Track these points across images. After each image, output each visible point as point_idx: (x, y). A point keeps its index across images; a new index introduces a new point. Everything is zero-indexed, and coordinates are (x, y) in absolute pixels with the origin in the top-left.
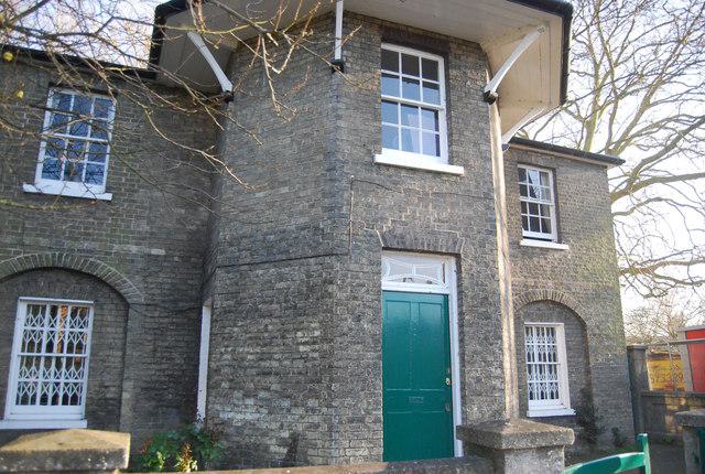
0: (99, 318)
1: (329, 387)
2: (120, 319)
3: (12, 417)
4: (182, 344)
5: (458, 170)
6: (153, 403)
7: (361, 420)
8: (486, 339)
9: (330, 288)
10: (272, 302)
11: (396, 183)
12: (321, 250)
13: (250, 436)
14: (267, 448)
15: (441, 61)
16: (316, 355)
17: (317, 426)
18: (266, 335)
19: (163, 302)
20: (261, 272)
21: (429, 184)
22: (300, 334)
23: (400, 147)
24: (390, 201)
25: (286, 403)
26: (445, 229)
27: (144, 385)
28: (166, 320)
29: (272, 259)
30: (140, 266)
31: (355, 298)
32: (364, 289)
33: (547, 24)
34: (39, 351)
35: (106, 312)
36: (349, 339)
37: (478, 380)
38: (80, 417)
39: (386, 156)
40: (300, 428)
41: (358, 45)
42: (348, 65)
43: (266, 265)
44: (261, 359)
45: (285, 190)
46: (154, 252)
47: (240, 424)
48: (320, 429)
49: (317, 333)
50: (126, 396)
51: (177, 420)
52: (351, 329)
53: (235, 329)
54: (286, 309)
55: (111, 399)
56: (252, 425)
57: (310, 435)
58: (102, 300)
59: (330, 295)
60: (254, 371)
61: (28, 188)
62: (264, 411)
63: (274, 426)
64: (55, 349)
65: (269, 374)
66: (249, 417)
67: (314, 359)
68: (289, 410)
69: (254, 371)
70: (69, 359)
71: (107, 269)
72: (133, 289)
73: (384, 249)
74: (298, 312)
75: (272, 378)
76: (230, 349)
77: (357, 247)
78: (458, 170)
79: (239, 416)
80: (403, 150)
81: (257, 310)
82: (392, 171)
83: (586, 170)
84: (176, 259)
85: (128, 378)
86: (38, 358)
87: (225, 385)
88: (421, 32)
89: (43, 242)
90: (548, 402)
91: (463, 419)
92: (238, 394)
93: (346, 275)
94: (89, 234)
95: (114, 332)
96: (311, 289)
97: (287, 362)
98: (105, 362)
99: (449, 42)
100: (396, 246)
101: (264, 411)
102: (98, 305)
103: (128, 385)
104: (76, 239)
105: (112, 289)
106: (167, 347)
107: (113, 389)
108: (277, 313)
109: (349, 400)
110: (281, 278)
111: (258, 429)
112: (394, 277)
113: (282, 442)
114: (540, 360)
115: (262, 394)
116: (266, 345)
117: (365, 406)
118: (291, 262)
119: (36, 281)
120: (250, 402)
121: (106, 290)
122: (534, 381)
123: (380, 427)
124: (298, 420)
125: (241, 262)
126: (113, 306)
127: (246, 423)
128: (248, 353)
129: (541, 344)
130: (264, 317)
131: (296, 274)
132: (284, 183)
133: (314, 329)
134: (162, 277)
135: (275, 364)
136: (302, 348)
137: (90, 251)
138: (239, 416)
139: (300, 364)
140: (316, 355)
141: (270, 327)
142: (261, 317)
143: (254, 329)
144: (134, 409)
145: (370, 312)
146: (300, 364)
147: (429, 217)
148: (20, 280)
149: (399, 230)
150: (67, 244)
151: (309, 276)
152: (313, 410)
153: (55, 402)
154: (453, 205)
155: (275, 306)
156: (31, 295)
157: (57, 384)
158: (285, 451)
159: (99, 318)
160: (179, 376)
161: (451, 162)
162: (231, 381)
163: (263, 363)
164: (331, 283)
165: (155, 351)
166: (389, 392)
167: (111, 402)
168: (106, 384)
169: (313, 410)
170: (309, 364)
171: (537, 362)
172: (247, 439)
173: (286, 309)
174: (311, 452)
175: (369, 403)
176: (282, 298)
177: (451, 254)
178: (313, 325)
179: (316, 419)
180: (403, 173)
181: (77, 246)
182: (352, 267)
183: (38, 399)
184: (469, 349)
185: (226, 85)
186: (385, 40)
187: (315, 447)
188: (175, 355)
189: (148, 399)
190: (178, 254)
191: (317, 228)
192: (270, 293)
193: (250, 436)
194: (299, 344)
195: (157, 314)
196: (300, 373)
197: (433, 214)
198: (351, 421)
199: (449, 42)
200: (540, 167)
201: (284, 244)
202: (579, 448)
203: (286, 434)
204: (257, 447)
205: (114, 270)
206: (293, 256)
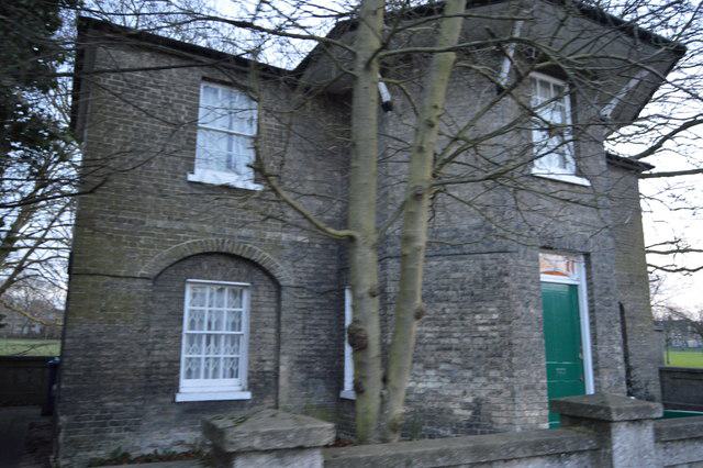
0: (255, 298)
1: (509, 361)
2: (272, 300)
4: (326, 322)
5: (586, 182)
6: (304, 375)
7: (533, 387)
9: (506, 280)
10: (448, 289)
12: (495, 248)
13: (433, 402)
14: (450, 412)
16: (494, 334)
17: (500, 392)
18: (444, 317)
19: (309, 284)
20: (435, 263)
22: (478, 316)
25: (468, 374)
27: (296, 358)
29: (445, 252)
30: (289, 252)
31: (524, 288)
32: (530, 281)
35: (261, 293)
38: (240, 388)
40: (483, 394)
43: (441, 258)
44: (441, 337)
46: (300, 239)
47: (422, 392)
48: (503, 395)
49: (495, 316)
50: (283, 369)
51: (324, 390)
54: (463, 295)
55: (268, 372)
56: (435, 392)
57: (493, 400)
58: (257, 283)
59: (506, 285)
60: (433, 347)
61: (191, 178)
62: (446, 380)
63: (457, 393)
65: (450, 349)
66: (430, 385)
68: (471, 380)
69: (433, 347)
70: (209, 336)
71: (262, 255)
72: (285, 273)
74: (475, 298)
75: (453, 353)
78: (259, 188)
81: (433, 296)
82: (542, 182)
84: (317, 246)
85: (284, 354)
86: (200, 336)
89: (208, 228)
90: (240, 363)
91: (596, 387)
94: (246, 223)
95: (268, 312)
96: (487, 279)
97: (467, 340)
98: (261, 338)
102: (255, 287)
103: (284, 359)
105: (266, 272)
106: (314, 325)
107: (268, 363)
109: (525, 372)
111: (441, 396)
113: (466, 406)
115: (443, 366)
116: (443, 325)
119: (200, 264)
120: (431, 373)
121: (259, 273)
123: (545, 393)
124: (480, 388)
126: (265, 288)
127: (428, 391)
128: (426, 332)
130: (441, 302)
131: (470, 268)
133: (493, 313)
134: (307, 262)
136: (481, 328)
137: (248, 238)
139: (480, 341)
140: (494, 334)
141: (448, 311)
142: (436, 301)
144: (290, 379)
146: (480, 341)
148: (190, 262)
150: (228, 231)
152: (495, 379)
155: (450, 293)
156: (204, 278)
157: (216, 359)
158: (470, 413)
159: (255, 298)
160: (325, 351)
163: (442, 341)
164: (507, 275)
165: (304, 328)
167: (268, 374)
168: (264, 358)
169: (495, 379)
170: (489, 342)
172: (430, 404)
173: (463, 295)
174: (495, 414)
176: (458, 286)
178: (491, 309)
179: (499, 386)
181: (237, 232)
182: (522, 262)
183: (211, 374)
184: (601, 329)
187: (499, 409)
188: (320, 332)
189: (301, 371)
190: (319, 241)
193: (433, 402)
194: (477, 325)
195: (305, 295)
196: (480, 349)
198: (526, 388)
203: (469, 399)
204: (441, 411)
205: (268, 255)
206: (467, 251)
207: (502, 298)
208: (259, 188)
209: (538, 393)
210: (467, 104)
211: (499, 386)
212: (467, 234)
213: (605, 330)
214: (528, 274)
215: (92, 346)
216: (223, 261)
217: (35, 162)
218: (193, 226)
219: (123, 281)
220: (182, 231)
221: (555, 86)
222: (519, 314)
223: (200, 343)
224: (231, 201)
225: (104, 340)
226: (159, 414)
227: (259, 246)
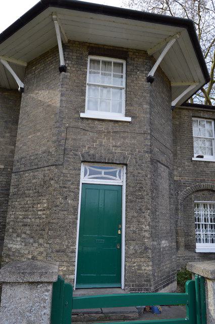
1: (48, 233)
3: (199, 248)
15: (124, 63)
16: (44, 216)
20: (27, 175)
21: (118, 128)
22: (39, 206)
23: (99, 109)
25: (31, 241)
26: (119, 150)
28: (3, 199)
31: (65, 187)
33: (179, 33)
34: (208, 222)
36: (60, 209)
39: (88, 114)
40: (36, 254)
41: (75, 57)
42: (69, 68)
43: (30, 171)
45: (39, 134)
49: (45, 205)
52: (61, 203)
53: (16, 203)
61: (82, 115)
63: (26, 252)
64: (209, 221)
66: (18, 247)
67: (44, 218)
73: (82, 162)
74: (40, 194)
75: (27, 228)
76: (14, 213)
77: (68, 161)
78: (129, 119)
79: (15, 246)
80: (112, 112)
82: (90, 121)
87: (11, 230)
88: (111, 48)
92: (15, 235)
93: (60, 176)
99: (128, 52)
100: (89, 160)
101: (23, 244)
106: (3, 212)
108: (31, 195)
109: (58, 240)
110: (34, 178)
112: (91, 176)
114: (205, 221)
115: (23, 236)
116: (26, 211)
117: (67, 244)
118: (38, 169)
120: (19, 239)
122: (201, 233)
125: (21, 170)
129: (206, 213)
131: (40, 174)
132: (39, 131)
135: (29, 220)
136: (39, 213)
138: (15, 246)
140: (44, 216)
141: (29, 202)
143: (23, 203)
145: (72, 194)
147: (109, 145)
149: (92, 152)
151: (44, 176)
153: (206, 242)
154: (124, 138)
161: (126, 116)
162: (13, 228)
163: (24, 220)
169: (41, 245)
170: (41, 221)
171: (210, 223)
175: (69, 242)
178: (44, 201)
179: (42, 249)
180: (96, 122)
182: (64, 171)
185: (20, 84)
186: (91, 53)
191: (49, 152)
192: (29, 185)
197: (112, 142)
198: (58, 251)
199: (128, 52)
200: (207, 118)
201: (36, 161)
206: (39, 166)
207: (49, 194)
208: (129, 119)
209: (66, 255)
210: (49, 81)
211: (42, 249)
212: (41, 156)
213: (136, 214)
214: (69, 179)
221: (114, 63)
222: (58, 203)
223: (199, 228)
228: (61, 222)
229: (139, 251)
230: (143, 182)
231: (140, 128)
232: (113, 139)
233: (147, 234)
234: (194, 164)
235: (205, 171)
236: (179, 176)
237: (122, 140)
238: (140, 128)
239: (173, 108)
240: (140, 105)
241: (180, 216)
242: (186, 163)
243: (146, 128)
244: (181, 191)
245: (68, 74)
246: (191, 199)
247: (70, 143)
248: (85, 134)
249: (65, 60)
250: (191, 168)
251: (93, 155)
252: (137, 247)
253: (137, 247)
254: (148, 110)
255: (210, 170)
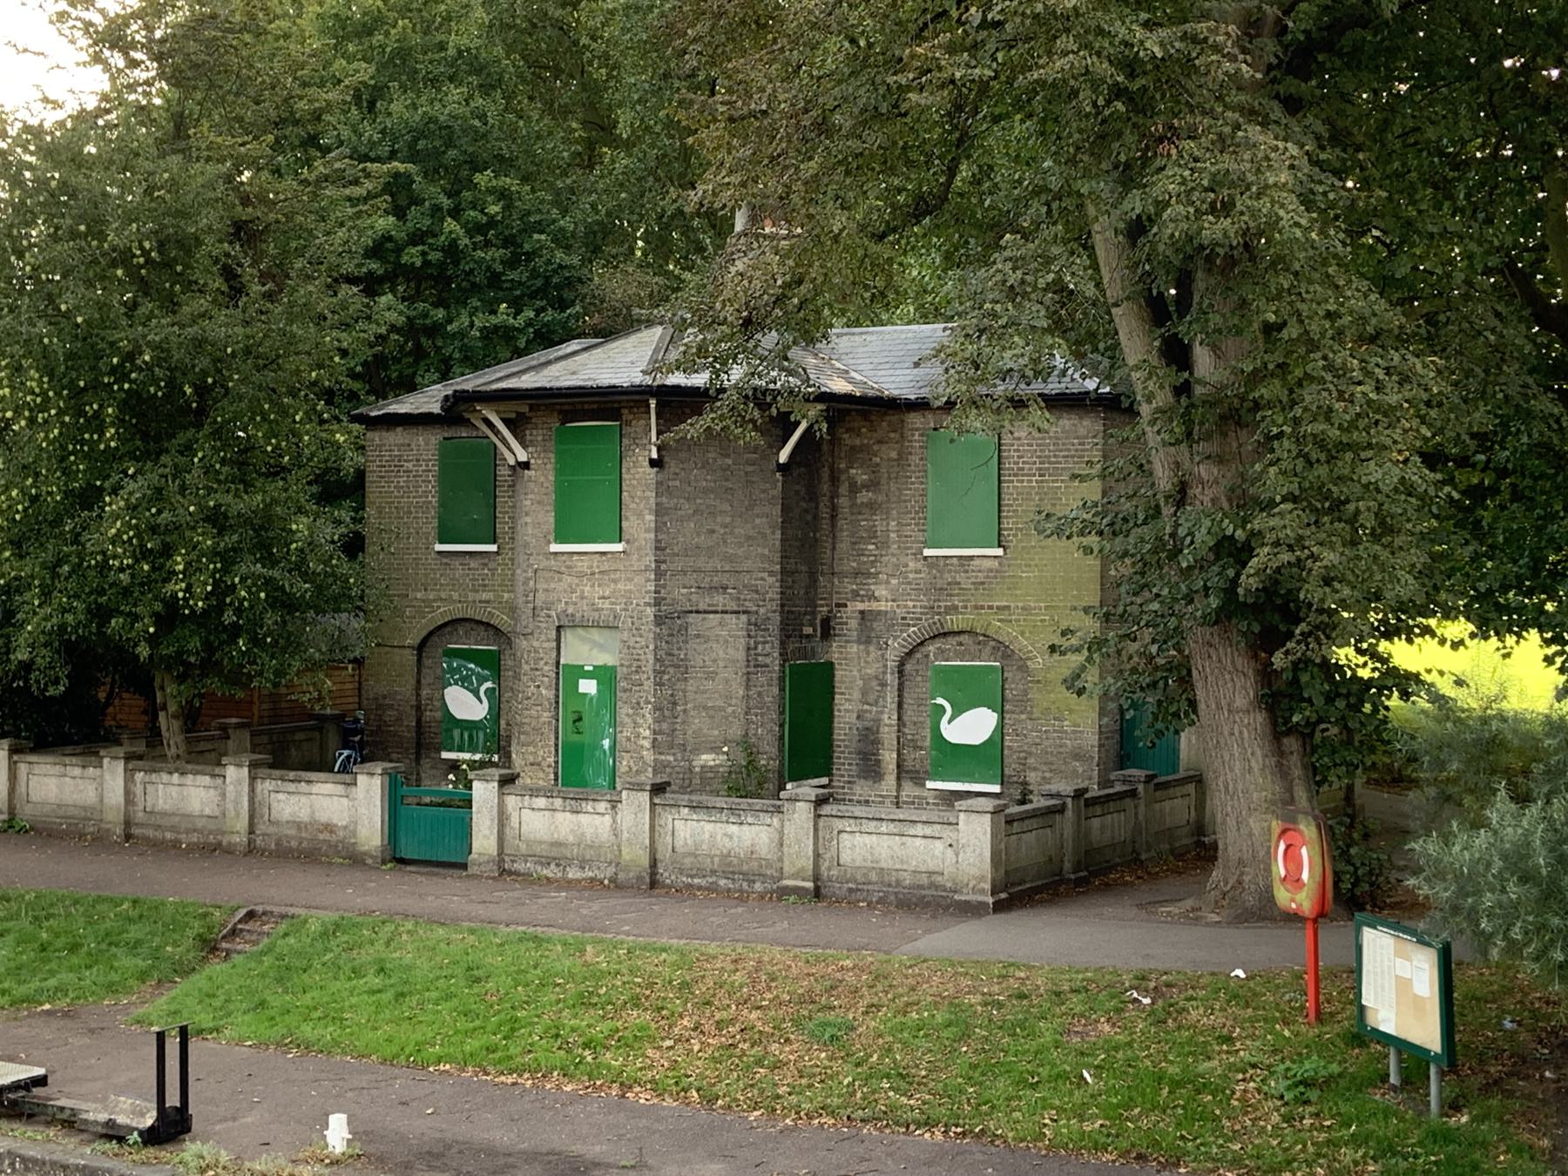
7: (539, 764)
8: (638, 703)
11: (569, 567)
24: (563, 585)
32: (542, 662)
37: (629, 739)
42: (532, 461)
83: (1081, 418)
104: (477, 591)
109: (531, 749)
148: (449, 629)
149: (570, 611)
154: (615, 581)
166: (469, 746)
177: (558, 641)
182: (536, 644)
197: (599, 591)
198: (532, 764)
202: (173, 751)
213: (631, 711)
215: (379, 707)
216: (475, 626)
217: (1023, 14)
218: (443, 595)
219: (396, 650)
220: (435, 601)
224: (472, 565)
225: (387, 701)
226: (432, 768)
227: (497, 609)
228: (534, 723)
229: (634, 769)
230: (643, 657)
231: (639, 560)
232: (599, 585)
233: (647, 744)
234: (931, 566)
235: (959, 583)
236: (893, 601)
237: (612, 585)
238: (639, 560)
239: (782, 468)
240: (640, 515)
241: (889, 700)
242: (912, 565)
243: (650, 560)
244: (895, 638)
245: (532, 473)
246: (927, 656)
247: (541, 596)
248: (560, 580)
249: (525, 447)
250: (922, 575)
251: (573, 615)
252: (632, 764)
253: (632, 764)
254: (653, 525)
255: (973, 580)
